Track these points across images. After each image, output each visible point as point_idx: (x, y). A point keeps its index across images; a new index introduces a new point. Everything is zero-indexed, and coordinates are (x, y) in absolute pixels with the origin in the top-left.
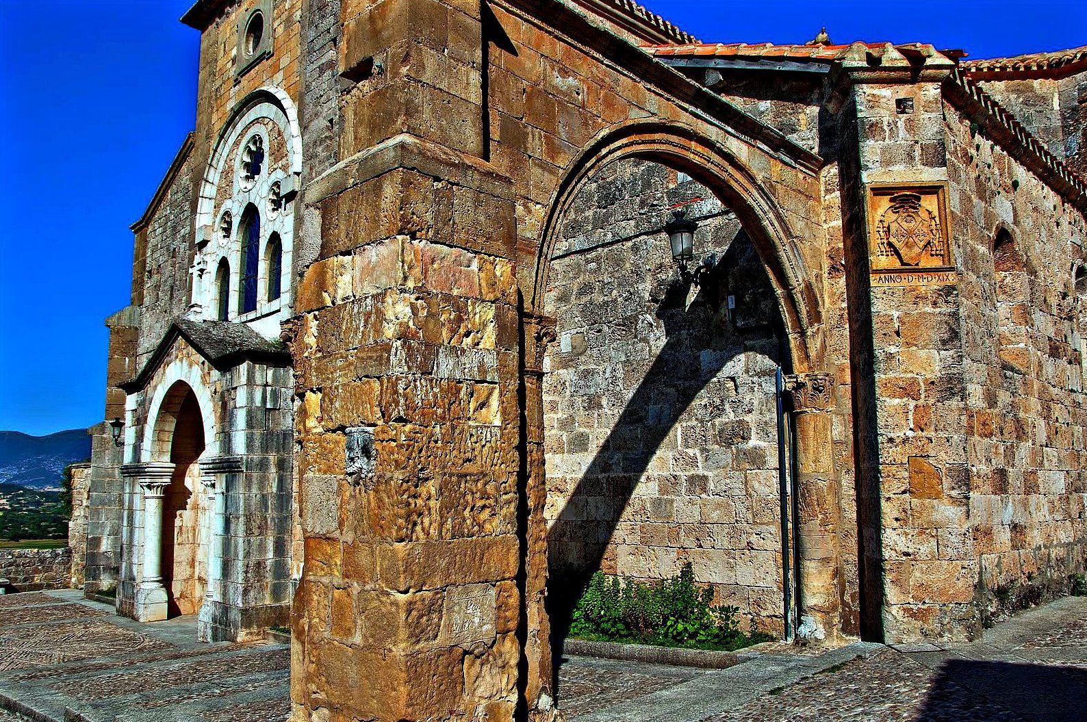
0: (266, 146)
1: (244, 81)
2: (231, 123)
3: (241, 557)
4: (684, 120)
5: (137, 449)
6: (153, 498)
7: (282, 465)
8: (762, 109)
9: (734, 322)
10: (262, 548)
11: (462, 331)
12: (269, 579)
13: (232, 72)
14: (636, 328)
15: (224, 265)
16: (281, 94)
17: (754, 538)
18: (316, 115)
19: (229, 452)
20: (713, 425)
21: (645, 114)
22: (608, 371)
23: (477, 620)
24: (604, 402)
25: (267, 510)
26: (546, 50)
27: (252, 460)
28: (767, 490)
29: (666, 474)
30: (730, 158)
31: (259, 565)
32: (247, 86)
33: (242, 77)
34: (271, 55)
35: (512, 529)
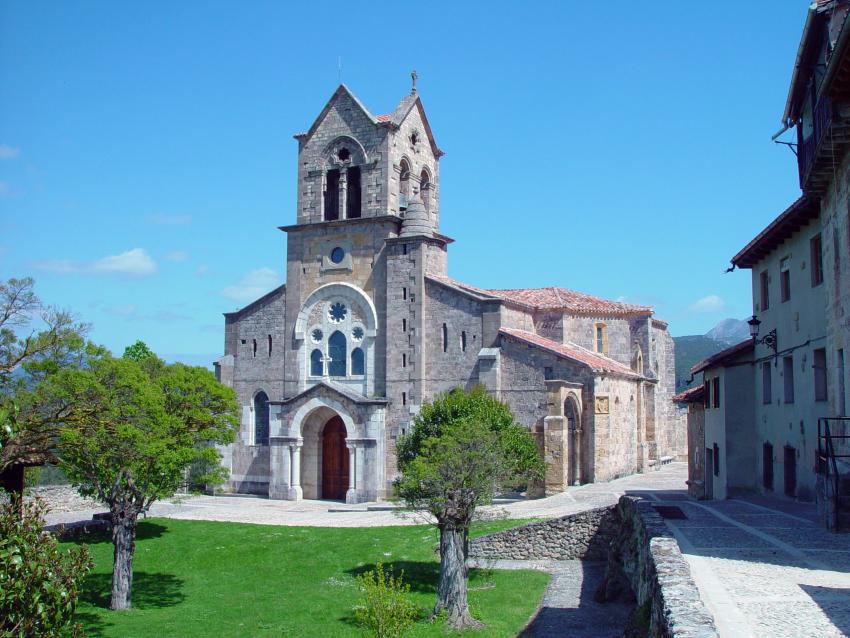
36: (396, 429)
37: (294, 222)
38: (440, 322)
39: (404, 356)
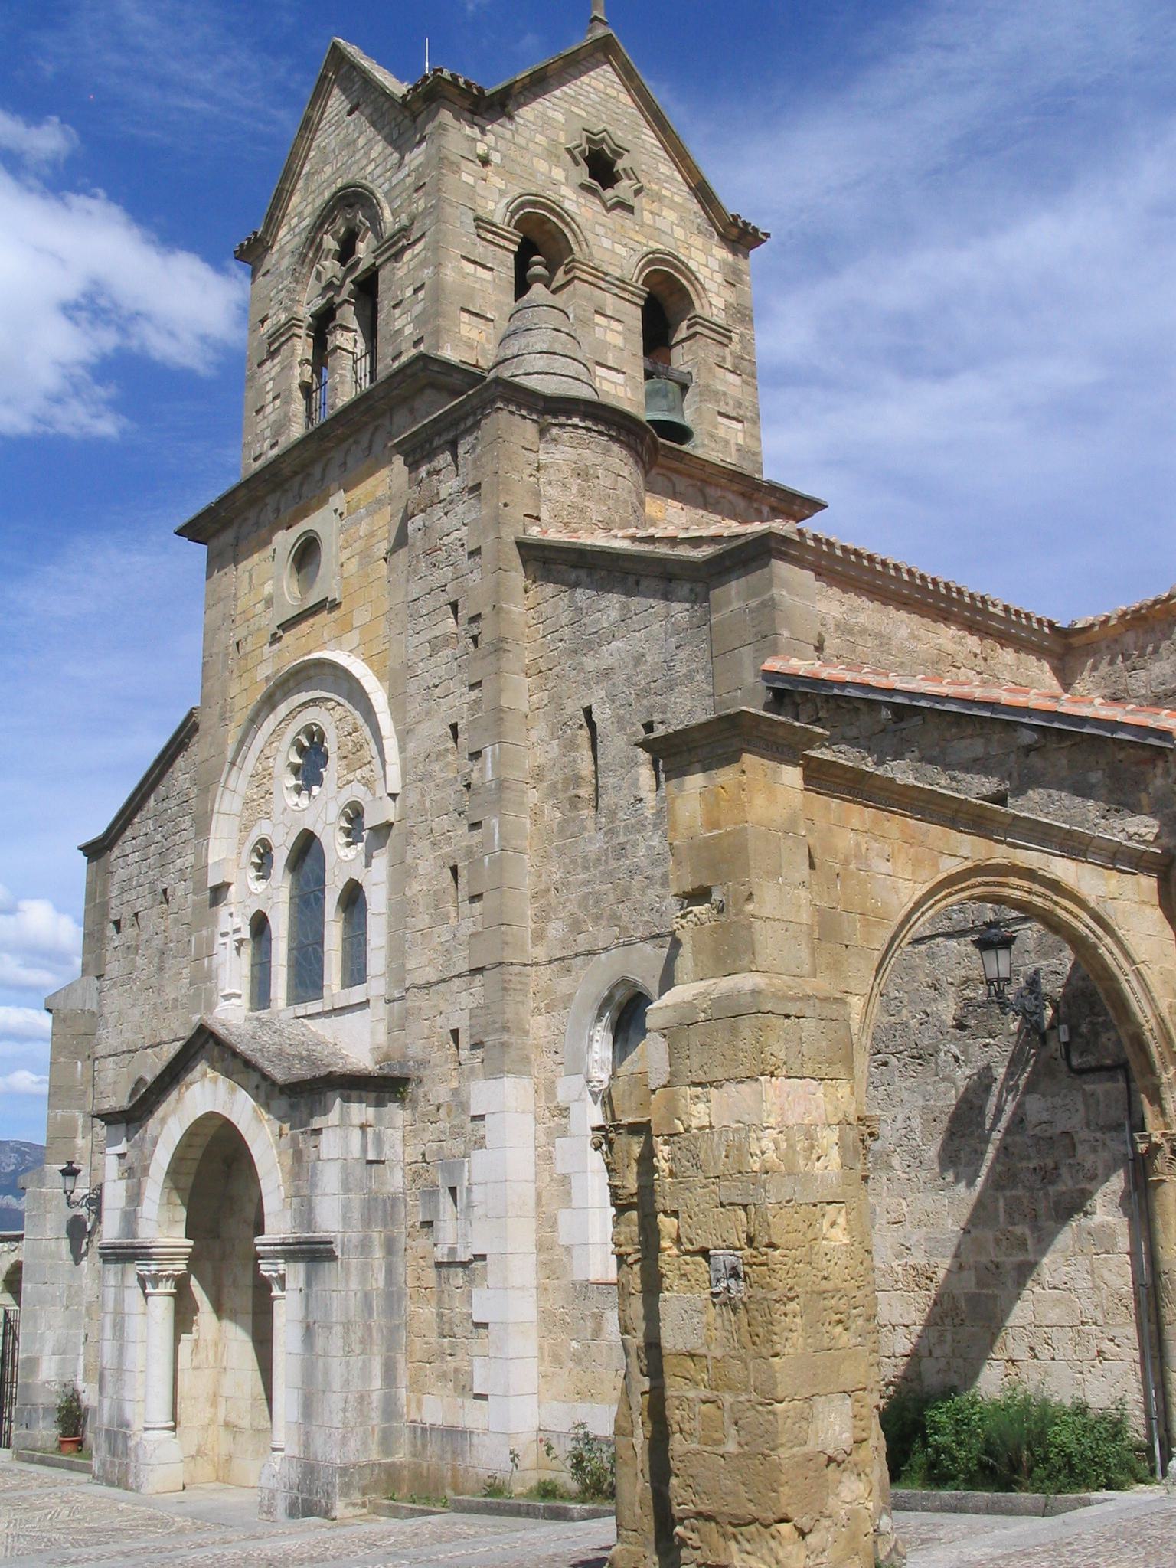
0: (331, 745)
1: (288, 638)
2: (269, 702)
3: (336, 1385)
4: (1001, 854)
5: (130, 1219)
6: (161, 1295)
7: (390, 1247)
8: (1093, 781)
9: (1068, 1059)
10: (365, 1374)
11: (814, 1157)
12: (376, 1418)
13: (270, 621)
14: (936, 1063)
15: (260, 924)
16: (358, 668)
17: (1107, 1346)
18: (428, 713)
19: (310, 1226)
20: (1046, 1194)
21: (957, 860)
22: (900, 1117)
23: (837, 1428)
24: (895, 1161)
25: (370, 1315)
26: (855, 823)
27: (349, 1241)
28: (1120, 1282)
29: (984, 1260)
30: (1054, 885)
31: (362, 1399)
32: (295, 650)
33: (284, 631)
34: (335, 605)
38: (573, 708)
39: (454, 870)
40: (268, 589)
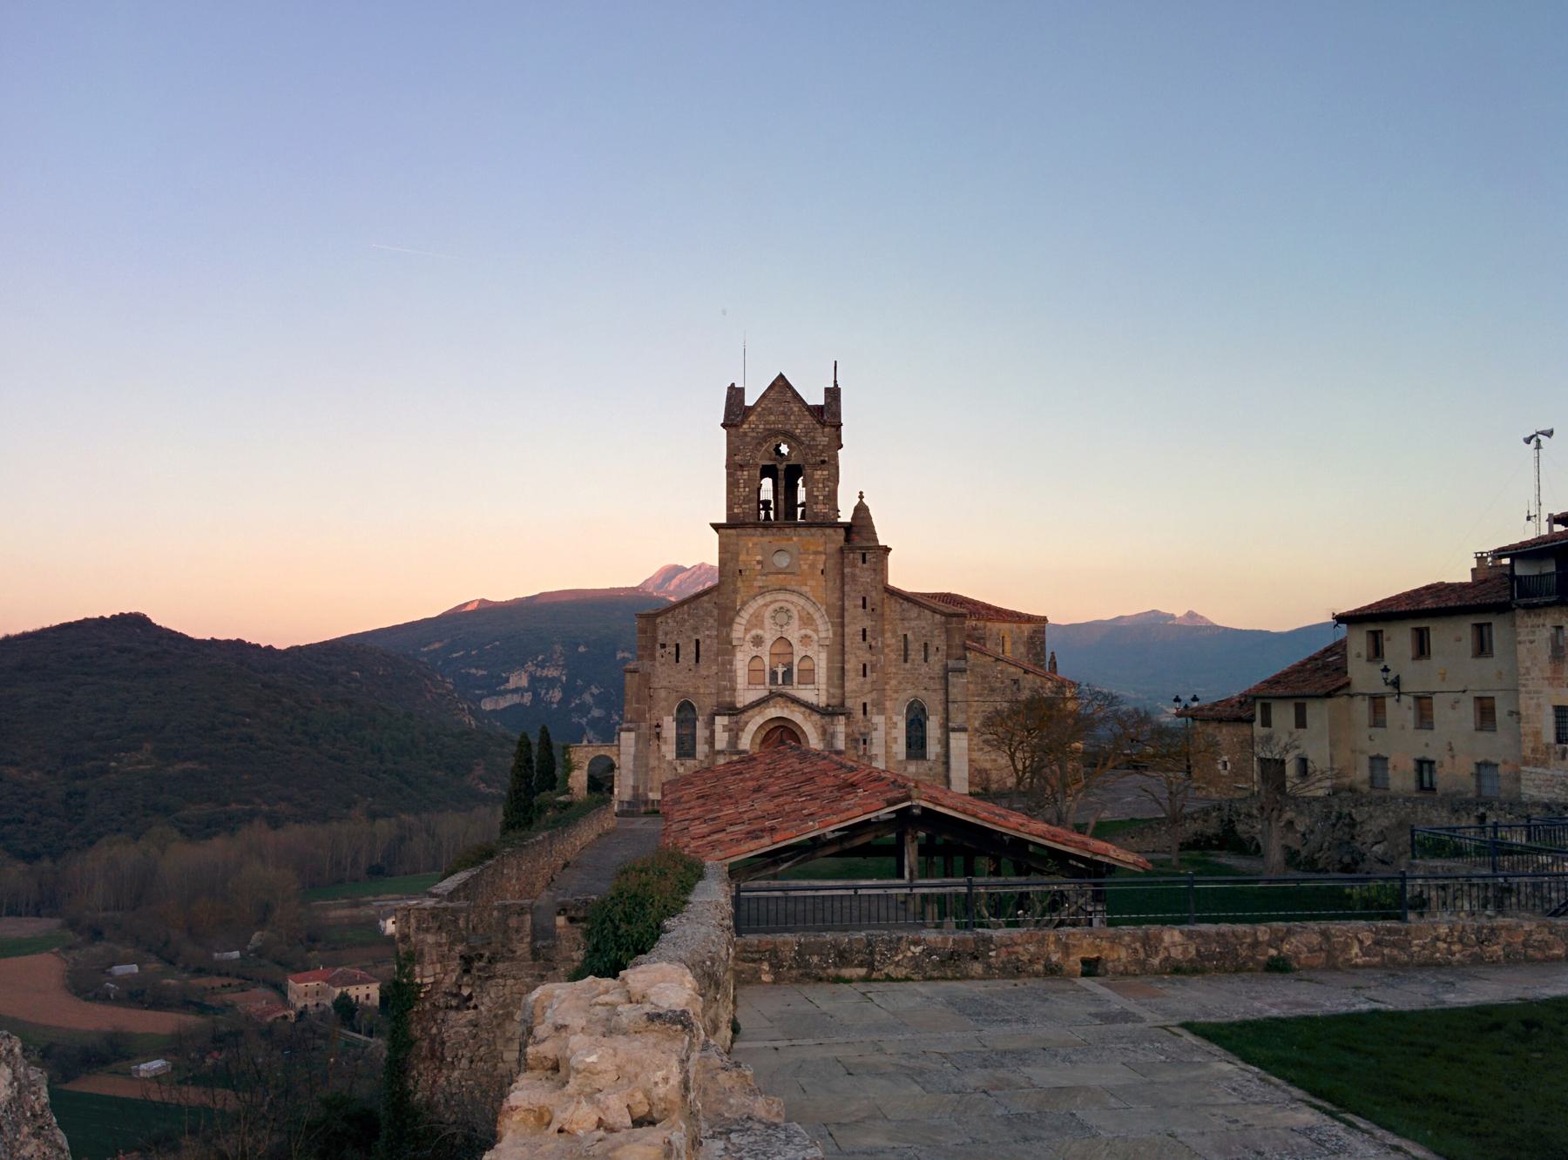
35: (952, 716)
36: (857, 741)
37: (723, 520)
40: (759, 558)
